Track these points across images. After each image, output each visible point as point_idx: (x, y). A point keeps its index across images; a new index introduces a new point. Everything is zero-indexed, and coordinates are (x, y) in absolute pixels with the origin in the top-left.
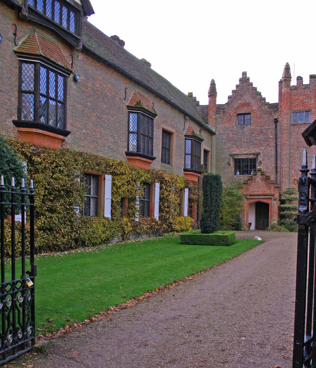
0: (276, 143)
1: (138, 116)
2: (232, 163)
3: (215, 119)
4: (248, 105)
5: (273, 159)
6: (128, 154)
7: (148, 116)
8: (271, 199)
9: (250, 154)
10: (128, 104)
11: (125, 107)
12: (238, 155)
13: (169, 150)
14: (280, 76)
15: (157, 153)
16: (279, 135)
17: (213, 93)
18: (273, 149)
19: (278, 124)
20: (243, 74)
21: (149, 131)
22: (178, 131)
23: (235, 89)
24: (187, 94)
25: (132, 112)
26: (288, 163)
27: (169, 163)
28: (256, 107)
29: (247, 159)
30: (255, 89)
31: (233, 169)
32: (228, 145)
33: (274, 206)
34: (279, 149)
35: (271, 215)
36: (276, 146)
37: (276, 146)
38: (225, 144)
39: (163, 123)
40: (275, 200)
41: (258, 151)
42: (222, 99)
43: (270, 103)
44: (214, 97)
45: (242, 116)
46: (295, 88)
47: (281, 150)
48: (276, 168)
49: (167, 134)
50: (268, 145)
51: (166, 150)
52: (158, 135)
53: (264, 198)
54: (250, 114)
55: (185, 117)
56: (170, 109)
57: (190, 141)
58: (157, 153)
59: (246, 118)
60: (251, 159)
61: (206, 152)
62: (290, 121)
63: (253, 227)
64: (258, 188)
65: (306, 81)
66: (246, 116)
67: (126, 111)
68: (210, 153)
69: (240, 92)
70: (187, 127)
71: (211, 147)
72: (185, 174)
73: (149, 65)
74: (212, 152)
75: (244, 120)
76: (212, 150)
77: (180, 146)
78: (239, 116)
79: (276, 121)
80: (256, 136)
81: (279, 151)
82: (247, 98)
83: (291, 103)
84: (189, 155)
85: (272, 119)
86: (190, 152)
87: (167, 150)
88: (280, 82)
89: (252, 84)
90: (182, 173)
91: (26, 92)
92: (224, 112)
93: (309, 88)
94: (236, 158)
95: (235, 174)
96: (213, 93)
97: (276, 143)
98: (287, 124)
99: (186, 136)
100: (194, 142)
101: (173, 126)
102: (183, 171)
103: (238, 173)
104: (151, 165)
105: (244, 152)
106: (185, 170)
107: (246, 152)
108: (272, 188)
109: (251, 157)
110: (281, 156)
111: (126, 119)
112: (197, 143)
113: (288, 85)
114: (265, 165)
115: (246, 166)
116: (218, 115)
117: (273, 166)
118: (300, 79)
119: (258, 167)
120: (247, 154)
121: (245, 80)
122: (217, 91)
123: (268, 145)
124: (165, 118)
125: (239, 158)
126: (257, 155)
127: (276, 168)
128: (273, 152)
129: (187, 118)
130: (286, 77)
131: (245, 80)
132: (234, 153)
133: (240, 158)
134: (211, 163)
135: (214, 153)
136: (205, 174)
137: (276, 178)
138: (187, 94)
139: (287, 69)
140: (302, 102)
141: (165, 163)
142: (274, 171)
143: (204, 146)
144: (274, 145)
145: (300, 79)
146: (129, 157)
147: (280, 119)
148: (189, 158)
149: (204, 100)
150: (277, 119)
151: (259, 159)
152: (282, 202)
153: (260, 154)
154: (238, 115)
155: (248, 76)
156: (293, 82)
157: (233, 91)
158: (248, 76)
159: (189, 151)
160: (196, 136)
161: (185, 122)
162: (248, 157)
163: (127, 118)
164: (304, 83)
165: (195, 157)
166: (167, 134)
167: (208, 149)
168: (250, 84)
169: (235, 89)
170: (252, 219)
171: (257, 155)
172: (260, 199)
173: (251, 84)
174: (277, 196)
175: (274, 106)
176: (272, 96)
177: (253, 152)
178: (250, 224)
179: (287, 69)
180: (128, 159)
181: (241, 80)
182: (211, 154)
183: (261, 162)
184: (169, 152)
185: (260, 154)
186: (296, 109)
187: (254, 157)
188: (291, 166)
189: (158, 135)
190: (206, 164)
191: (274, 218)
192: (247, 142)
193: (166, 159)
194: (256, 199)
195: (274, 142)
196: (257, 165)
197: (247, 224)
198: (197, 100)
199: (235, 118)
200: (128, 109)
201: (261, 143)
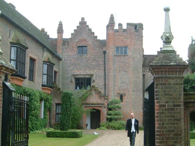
0: (105, 68)
1: (17, 49)
2: (74, 81)
3: (63, 49)
4: (85, 40)
5: (103, 79)
6: (43, 86)
7: (21, 49)
8: (102, 107)
9: (86, 75)
10: (11, 41)
11: (9, 43)
12: (78, 75)
13: (33, 71)
14: (107, 22)
15: (27, 74)
16: (106, 62)
17: (60, 30)
18: (103, 72)
19: (106, 55)
20: (82, 19)
21: (22, 59)
22: (39, 58)
23: (76, 28)
24: (40, 29)
25: (13, 46)
26: (113, 81)
27: (32, 81)
28: (91, 42)
29: (85, 78)
30: (90, 30)
31: (74, 85)
32: (71, 68)
33: (104, 112)
34: (106, 72)
35: (102, 119)
36: (105, 70)
37: (105, 70)
38: (69, 67)
39: (30, 53)
40: (105, 107)
41: (92, 73)
42: (67, 35)
43: (98, 38)
44: (62, 34)
45: (81, 48)
46: (117, 31)
47: (108, 73)
48: (105, 85)
49: (32, 60)
50: (99, 69)
51: (32, 71)
52: (28, 61)
53: (97, 106)
54: (86, 46)
55: (43, 49)
56: (35, 43)
57: (46, 66)
58: (27, 74)
59: (84, 50)
60: (87, 78)
61: (56, 72)
62: (114, 53)
63: (89, 127)
64: (94, 99)
65: (125, 27)
66: (84, 47)
67: (9, 45)
68: (58, 73)
69: (79, 31)
70: (12, 37)
71: (59, 69)
72: (42, 88)
73: (14, 8)
74: (59, 72)
75: (82, 51)
76: (59, 71)
77: (41, 70)
78: (79, 48)
79: (105, 53)
80: (91, 62)
81: (107, 73)
82: (85, 36)
83: (115, 40)
84: (46, 75)
85: (102, 51)
86: (46, 73)
87: (32, 72)
88: (108, 26)
89: (93, 33)
90: (40, 88)
91: (44, 74)
92: (68, 45)
93: (126, 31)
94: (77, 77)
95: (76, 89)
96: (60, 30)
97: (105, 68)
98: (112, 55)
99: (44, 61)
100: (19, 50)
101: (36, 55)
102: (41, 86)
103: (78, 88)
104: (23, 82)
105: (82, 73)
106: (43, 86)
107: (84, 74)
108: (103, 99)
109: (87, 77)
110: (108, 77)
111: (9, 51)
112: (22, 51)
113: (113, 29)
114: (98, 82)
115: (83, 82)
116: (64, 47)
117: (103, 83)
118: (120, 25)
119: (92, 84)
120: (84, 75)
121: (83, 23)
122: (64, 29)
123: (99, 69)
124: (33, 52)
125: (78, 77)
126: (92, 75)
127: (105, 85)
128: (103, 74)
129: (45, 49)
130: (112, 23)
131: (83, 23)
132: (75, 73)
133: (80, 77)
134: (59, 79)
135: (61, 73)
136: (180, 129)
137: (105, 92)
138: (40, 29)
139: (112, 18)
140: (122, 41)
141: (30, 80)
142: (103, 87)
143: (55, 69)
144: (104, 69)
145: (120, 25)
146: (43, 87)
147: (107, 52)
148: (45, 77)
149: (53, 34)
150: (105, 51)
151: (93, 79)
152: (110, 109)
153: (93, 75)
154: (78, 47)
155: (85, 21)
156: (116, 27)
157: (75, 30)
158: (85, 21)
159: (45, 72)
160: (50, 62)
161: (43, 52)
162: (85, 77)
163: (10, 50)
164: (123, 28)
165: (49, 76)
166: (32, 60)
167: (57, 70)
168: (85, 22)
169: (76, 28)
170: (88, 121)
171: (92, 75)
172: (94, 107)
173: (88, 26)
174: (106, 104)
175: (103, 43)
176: (101, 34)
177: (89, 73)
178: (87, 125)
179: (112, 18)
180: (42, 88)
181: (80, 23)
182: (59, 74)
183: (94, 81)
184: (33, 72)
185: (93, 75)
186: (118, 45)
187: (90, 77)
188: (115, 84)
189: (28, 61)
190: (55, 81)
191: (104, 120)
192: (84, 66)
193: (31, 78)
194: (91, 107)
195: (104, 67)
196: (92, 82)
197: (85, 125)
198: (48, 34)
199: (76, 49)
200: (11, 44)
201: (94, 67)
